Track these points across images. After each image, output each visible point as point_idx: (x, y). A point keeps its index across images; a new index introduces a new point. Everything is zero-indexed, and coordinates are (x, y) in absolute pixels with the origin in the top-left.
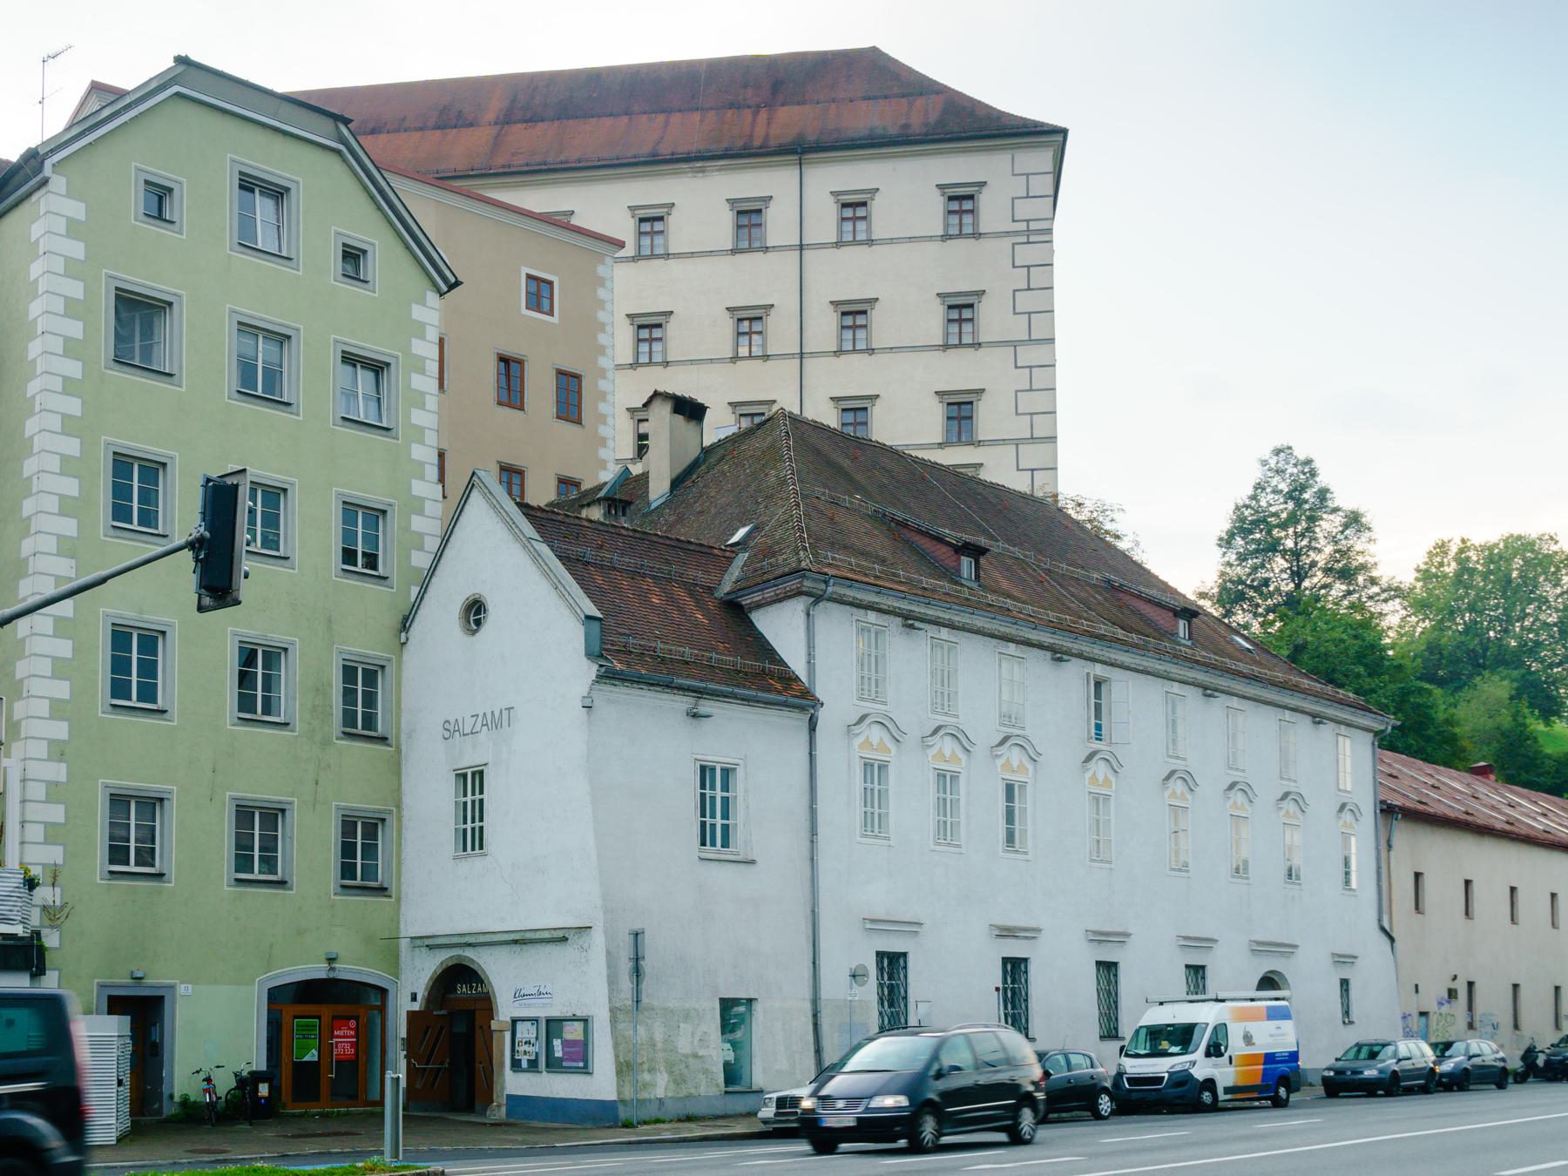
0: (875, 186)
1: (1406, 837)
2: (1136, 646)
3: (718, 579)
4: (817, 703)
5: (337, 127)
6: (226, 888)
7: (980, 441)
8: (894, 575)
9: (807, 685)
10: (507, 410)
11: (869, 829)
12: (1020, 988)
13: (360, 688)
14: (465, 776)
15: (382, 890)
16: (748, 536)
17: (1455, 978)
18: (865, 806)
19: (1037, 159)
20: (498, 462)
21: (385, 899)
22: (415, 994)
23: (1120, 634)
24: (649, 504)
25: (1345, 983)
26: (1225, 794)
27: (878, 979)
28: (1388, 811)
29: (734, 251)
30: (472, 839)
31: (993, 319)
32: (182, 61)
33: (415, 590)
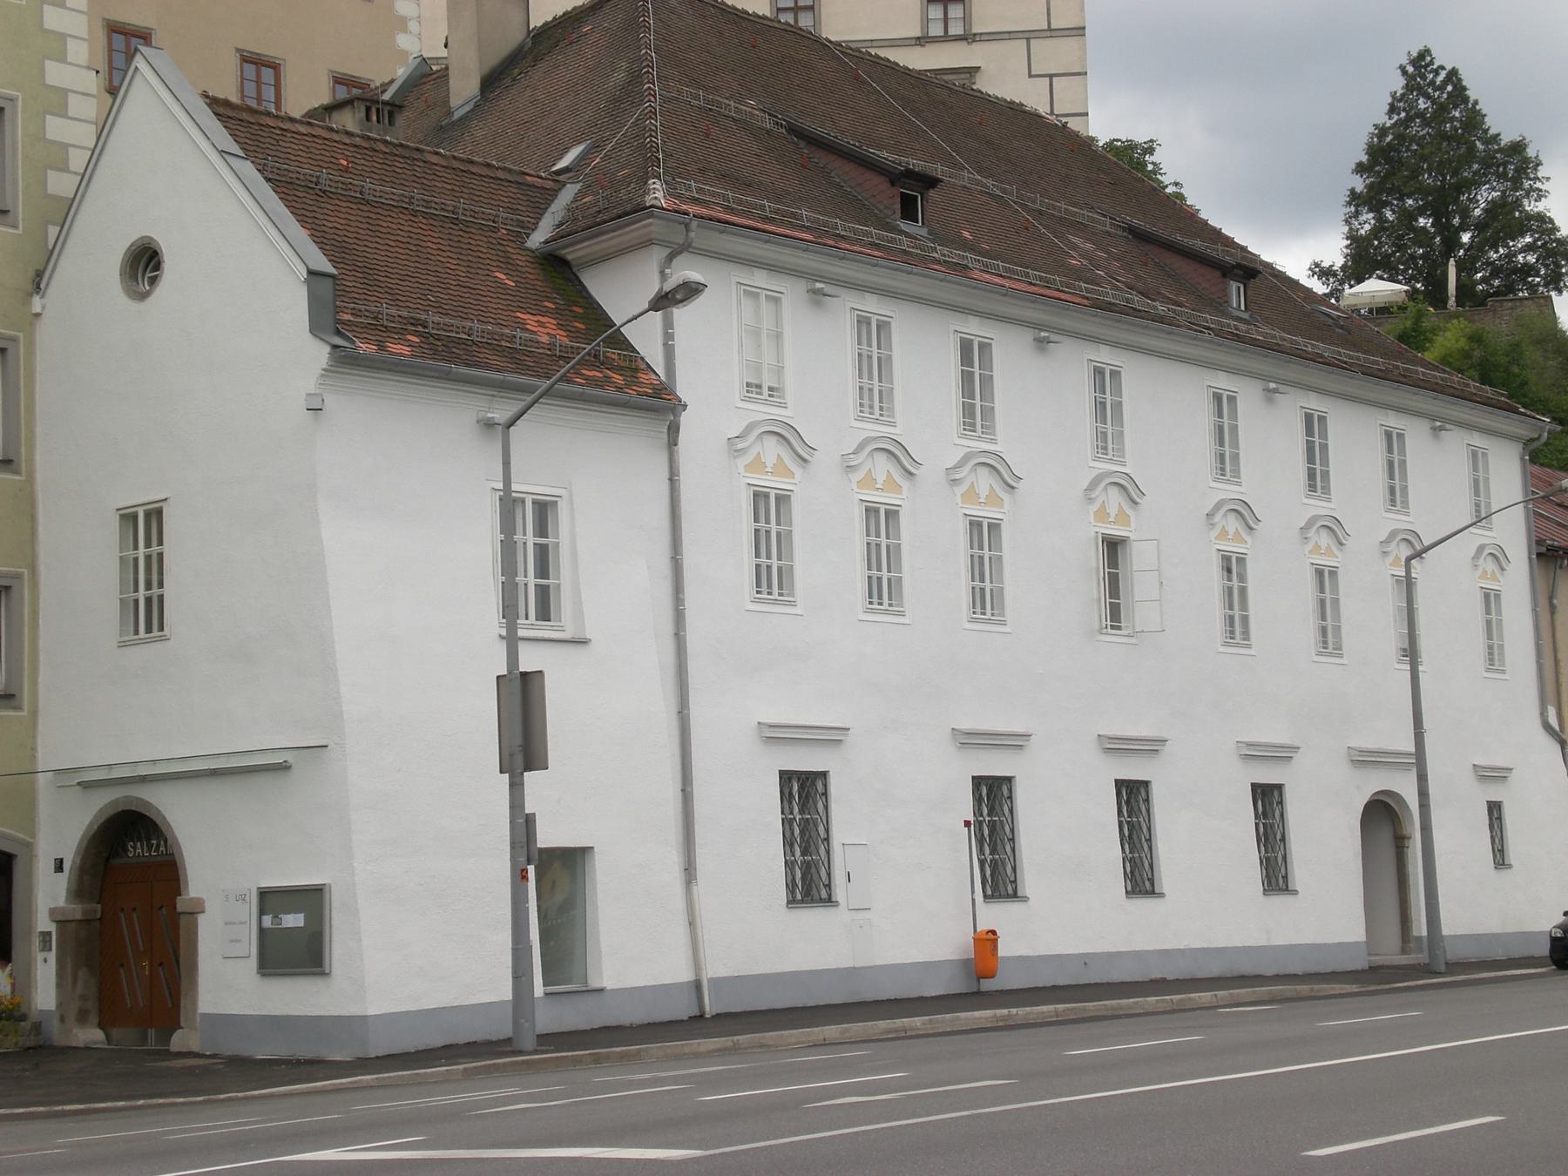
2: (1161, 319)
3: (532, 220)
4: (677, 407)
7: (975, 34)
8: (793, 215)
9: (663, 378)
11: (764, 588)
12: (1001, 822)
14: (135, 517)
16: (582, 157)
20: (238, 50)
21: (11, 713)
22: (61, 861)
23: (1137, 301)
24: (450, 113)
25: (1495, 809)
26: (1302, 533)
27: (782, 813)
33: (53, 231)
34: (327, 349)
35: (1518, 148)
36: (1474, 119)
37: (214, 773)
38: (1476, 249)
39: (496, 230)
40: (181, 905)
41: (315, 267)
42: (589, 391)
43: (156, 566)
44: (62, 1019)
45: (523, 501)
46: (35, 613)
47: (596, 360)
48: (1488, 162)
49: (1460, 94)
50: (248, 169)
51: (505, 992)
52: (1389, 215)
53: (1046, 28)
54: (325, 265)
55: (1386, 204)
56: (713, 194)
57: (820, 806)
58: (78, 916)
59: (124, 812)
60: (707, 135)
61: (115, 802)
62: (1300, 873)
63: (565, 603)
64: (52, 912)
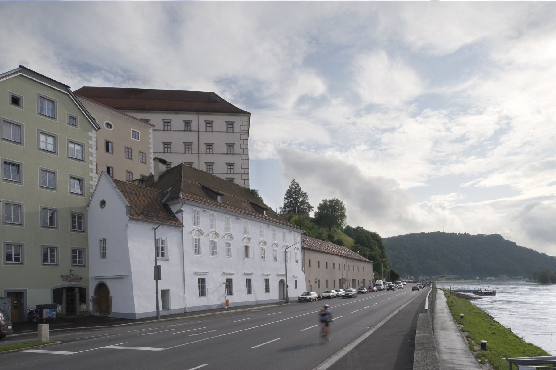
0: (213, 120)
1: (307, 254)
4: (183, 226)
5: (67, 89)
6: (40, 266)
10: (128, 160)
13: (77, 220)
14: (102, 240)
15: (84, 266)
16: (171, 190)
17: (316, 279)
18: (195, 248)
19: (245, 118)
25: (296, 281)
28: (304, 248)
29: (185, 131)
30: (104, 254)
31: (237, 149)
32: (20, 66)
33: (90, 198)
34: (129, 217)
35: (305, 194)
36: (300, 189)
37: (113, 278)
38: (299, 206)
39: (157, 200)
40: (109, 297)
41: (127, 205)
42: (170, 224)
43: (105, 247)
44: (94, 311)
45: (159, 240)
46: (88, 254)
47: (171, 219)
48: (302, 195)
49: (298, 186)
50: (118, 190)
51: (155, 310)
52: (289, 200)
53: (244, 173)
54: (129, 205)
55: (289, 199)
56: (190, 196)
57: (204, 283)
58: (95, 297)
59: (100, 283)
60: (190, 187)
61: (100, 282)
62: (271, 290)
63: (166, 254)
64: (92, 297)
